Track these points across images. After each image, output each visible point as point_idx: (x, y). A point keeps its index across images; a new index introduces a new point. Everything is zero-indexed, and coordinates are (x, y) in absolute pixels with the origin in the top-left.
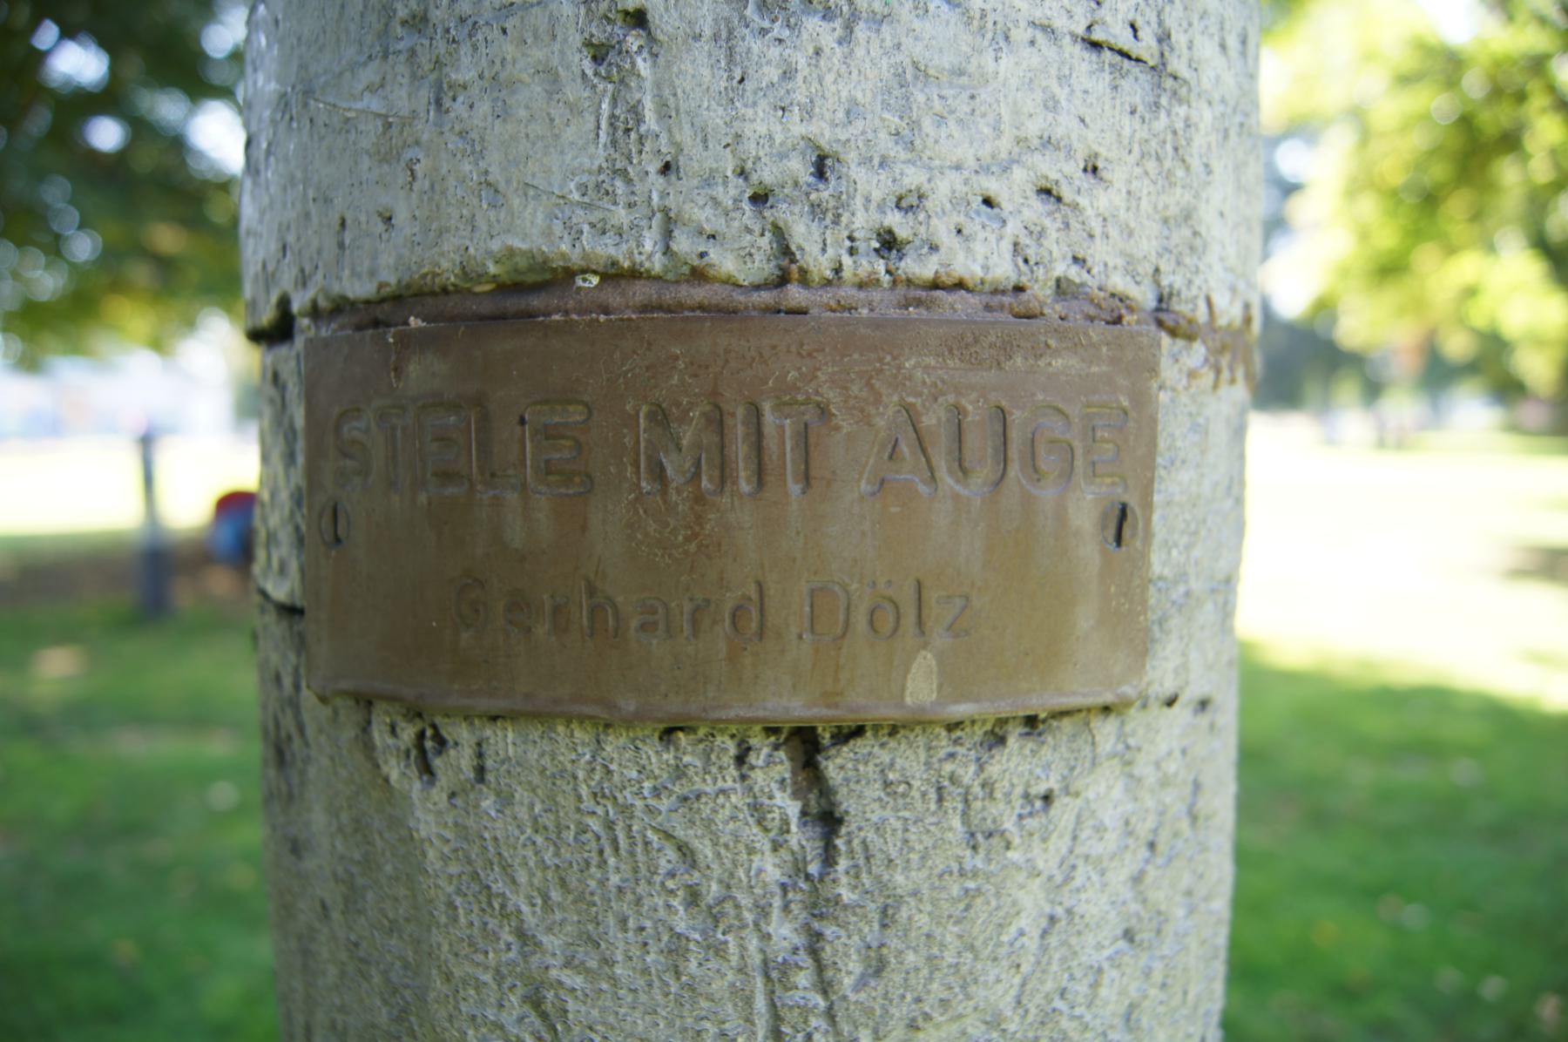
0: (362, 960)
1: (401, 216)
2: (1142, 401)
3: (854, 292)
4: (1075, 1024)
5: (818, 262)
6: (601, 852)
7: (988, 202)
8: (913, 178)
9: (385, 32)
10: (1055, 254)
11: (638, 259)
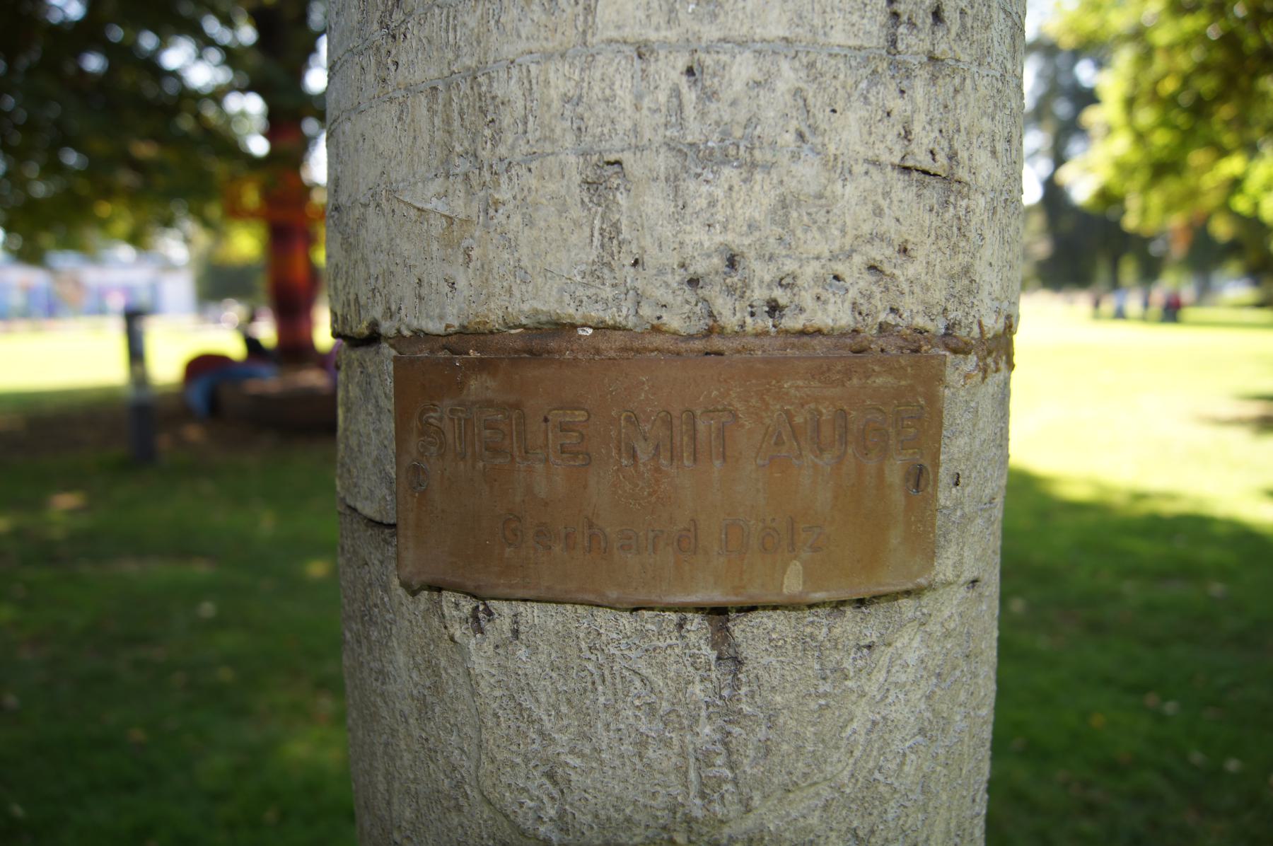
0: (430, 750)
1: (461, 283)
2: (933, 400)
3: (752, 340)
4: (887, 788)
5: (729, 320)
6: (594, 683)
7: (836, 278)
8: (790, 266)
9: (446, 161)
10: (880, 307)
11: (618, 319)
